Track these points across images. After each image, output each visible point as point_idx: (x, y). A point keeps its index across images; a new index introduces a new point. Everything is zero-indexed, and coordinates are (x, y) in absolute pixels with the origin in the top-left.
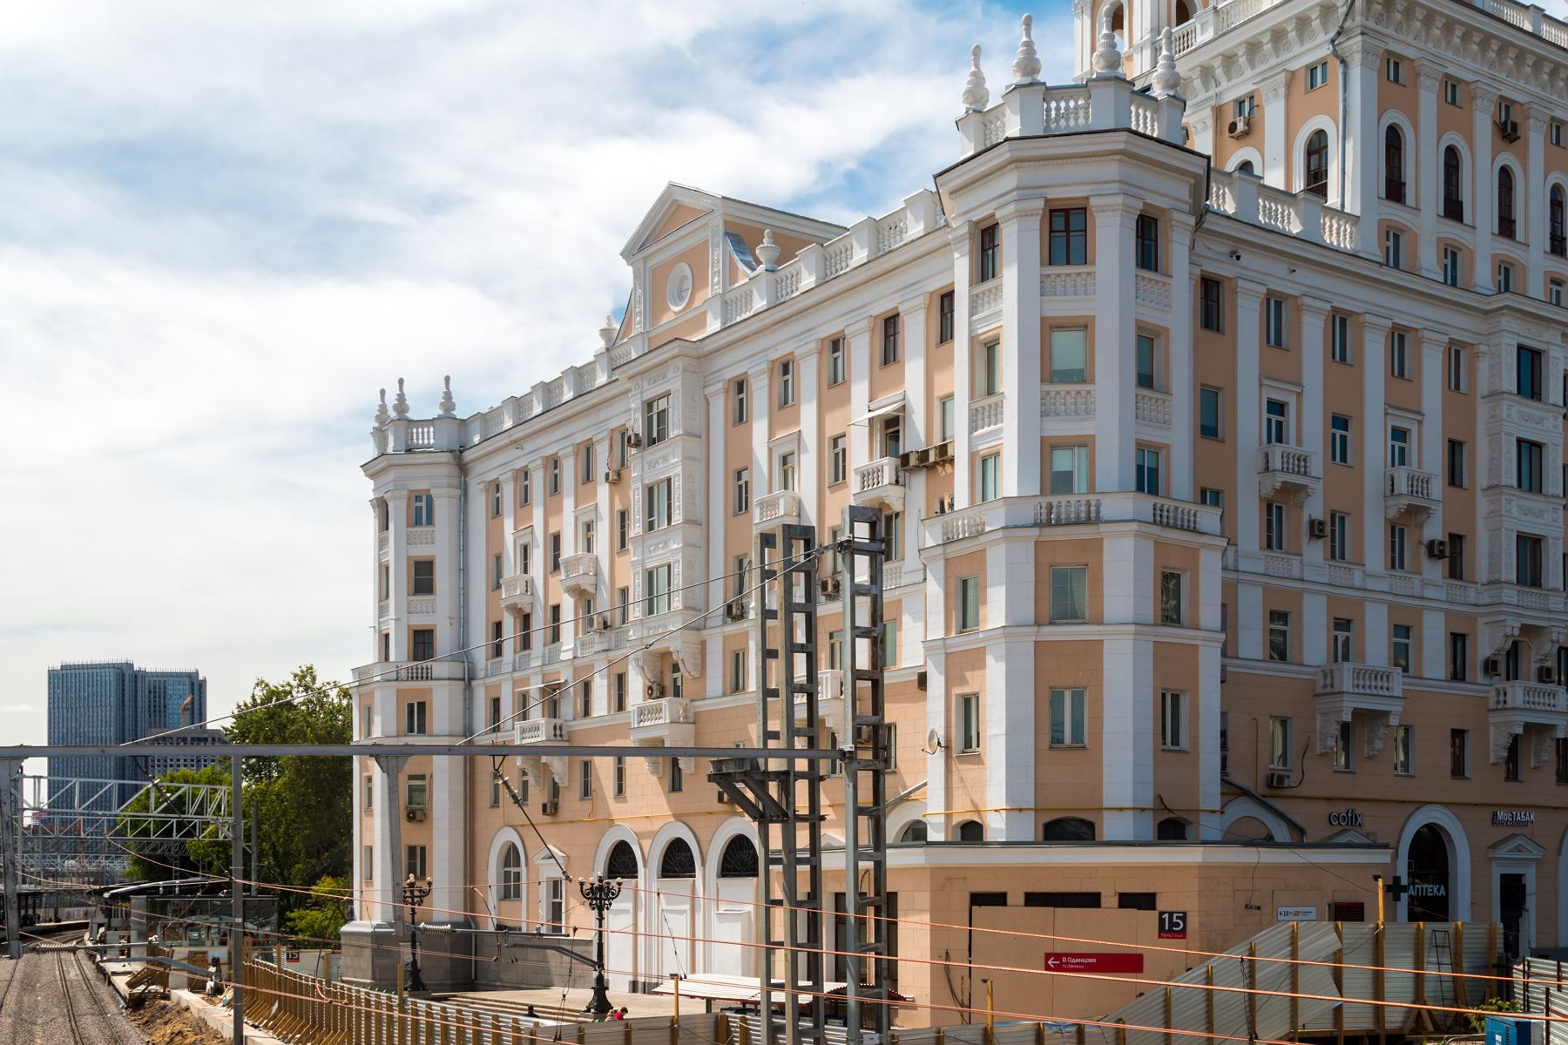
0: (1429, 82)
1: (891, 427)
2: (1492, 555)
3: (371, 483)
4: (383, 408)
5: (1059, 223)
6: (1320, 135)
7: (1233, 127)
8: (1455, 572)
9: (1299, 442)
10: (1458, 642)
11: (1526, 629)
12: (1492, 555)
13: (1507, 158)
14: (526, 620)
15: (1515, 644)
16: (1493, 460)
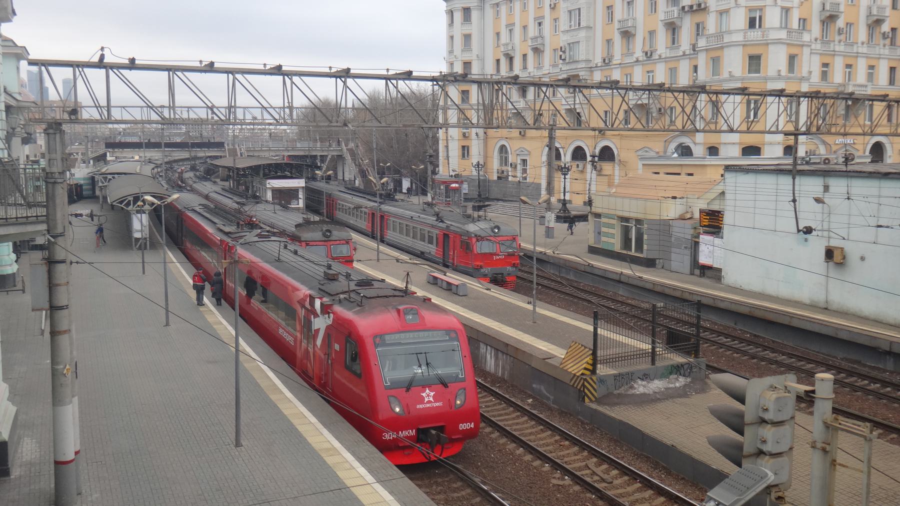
8: (893, 43)
14: (511, 59)
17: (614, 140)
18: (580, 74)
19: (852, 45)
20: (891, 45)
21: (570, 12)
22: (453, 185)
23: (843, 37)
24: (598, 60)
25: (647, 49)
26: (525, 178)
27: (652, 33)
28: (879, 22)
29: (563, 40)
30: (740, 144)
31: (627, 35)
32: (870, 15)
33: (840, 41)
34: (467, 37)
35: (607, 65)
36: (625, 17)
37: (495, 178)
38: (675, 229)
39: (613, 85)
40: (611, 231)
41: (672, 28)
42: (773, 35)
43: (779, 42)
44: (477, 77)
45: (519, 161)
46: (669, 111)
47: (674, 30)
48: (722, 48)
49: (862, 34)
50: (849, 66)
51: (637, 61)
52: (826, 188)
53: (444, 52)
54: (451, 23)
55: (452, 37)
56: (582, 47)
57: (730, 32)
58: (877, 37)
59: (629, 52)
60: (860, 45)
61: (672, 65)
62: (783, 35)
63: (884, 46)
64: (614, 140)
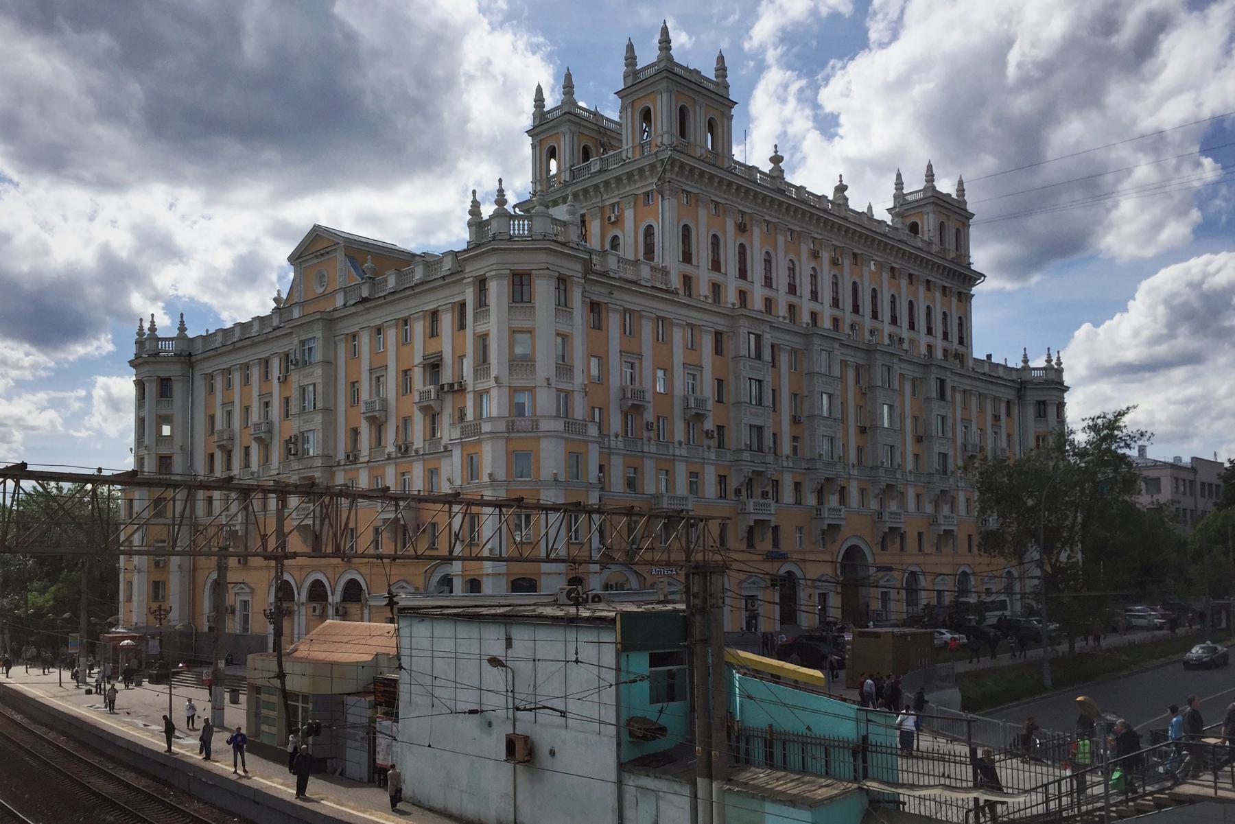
0: (355, 744)
1: (433, 366)
2: (739, 436)
4: (141, 328)
5: (517, 280)
6: (650, 227)
7: (609, 218)
8: (721, 445)
9: (641, 384)
10: (722, 479)
12: (739, 436)
13: (742, 240)
14: (229, 454)
15: (750, 480)
17: (363, 570)
20: (719, 447)
23: (653, 434)
24: (341, 456)
27: (407, 421)
28: (700, 417)
30: (507, 574)
31: (378, 424)
32: (687, 407)
33: (649, 440)
37: (206, 629)
39: (383, 494)
40: (273, 714)
41: (432, 416)
42: (546, 425)
44: (178, 478)
45: (238, 605)
46: (429, 530)
47: (434, 416)
51: (389, 458)
52: (509, 643)
60: (677, 445)
63: (709, 448)
64: (363, 570)
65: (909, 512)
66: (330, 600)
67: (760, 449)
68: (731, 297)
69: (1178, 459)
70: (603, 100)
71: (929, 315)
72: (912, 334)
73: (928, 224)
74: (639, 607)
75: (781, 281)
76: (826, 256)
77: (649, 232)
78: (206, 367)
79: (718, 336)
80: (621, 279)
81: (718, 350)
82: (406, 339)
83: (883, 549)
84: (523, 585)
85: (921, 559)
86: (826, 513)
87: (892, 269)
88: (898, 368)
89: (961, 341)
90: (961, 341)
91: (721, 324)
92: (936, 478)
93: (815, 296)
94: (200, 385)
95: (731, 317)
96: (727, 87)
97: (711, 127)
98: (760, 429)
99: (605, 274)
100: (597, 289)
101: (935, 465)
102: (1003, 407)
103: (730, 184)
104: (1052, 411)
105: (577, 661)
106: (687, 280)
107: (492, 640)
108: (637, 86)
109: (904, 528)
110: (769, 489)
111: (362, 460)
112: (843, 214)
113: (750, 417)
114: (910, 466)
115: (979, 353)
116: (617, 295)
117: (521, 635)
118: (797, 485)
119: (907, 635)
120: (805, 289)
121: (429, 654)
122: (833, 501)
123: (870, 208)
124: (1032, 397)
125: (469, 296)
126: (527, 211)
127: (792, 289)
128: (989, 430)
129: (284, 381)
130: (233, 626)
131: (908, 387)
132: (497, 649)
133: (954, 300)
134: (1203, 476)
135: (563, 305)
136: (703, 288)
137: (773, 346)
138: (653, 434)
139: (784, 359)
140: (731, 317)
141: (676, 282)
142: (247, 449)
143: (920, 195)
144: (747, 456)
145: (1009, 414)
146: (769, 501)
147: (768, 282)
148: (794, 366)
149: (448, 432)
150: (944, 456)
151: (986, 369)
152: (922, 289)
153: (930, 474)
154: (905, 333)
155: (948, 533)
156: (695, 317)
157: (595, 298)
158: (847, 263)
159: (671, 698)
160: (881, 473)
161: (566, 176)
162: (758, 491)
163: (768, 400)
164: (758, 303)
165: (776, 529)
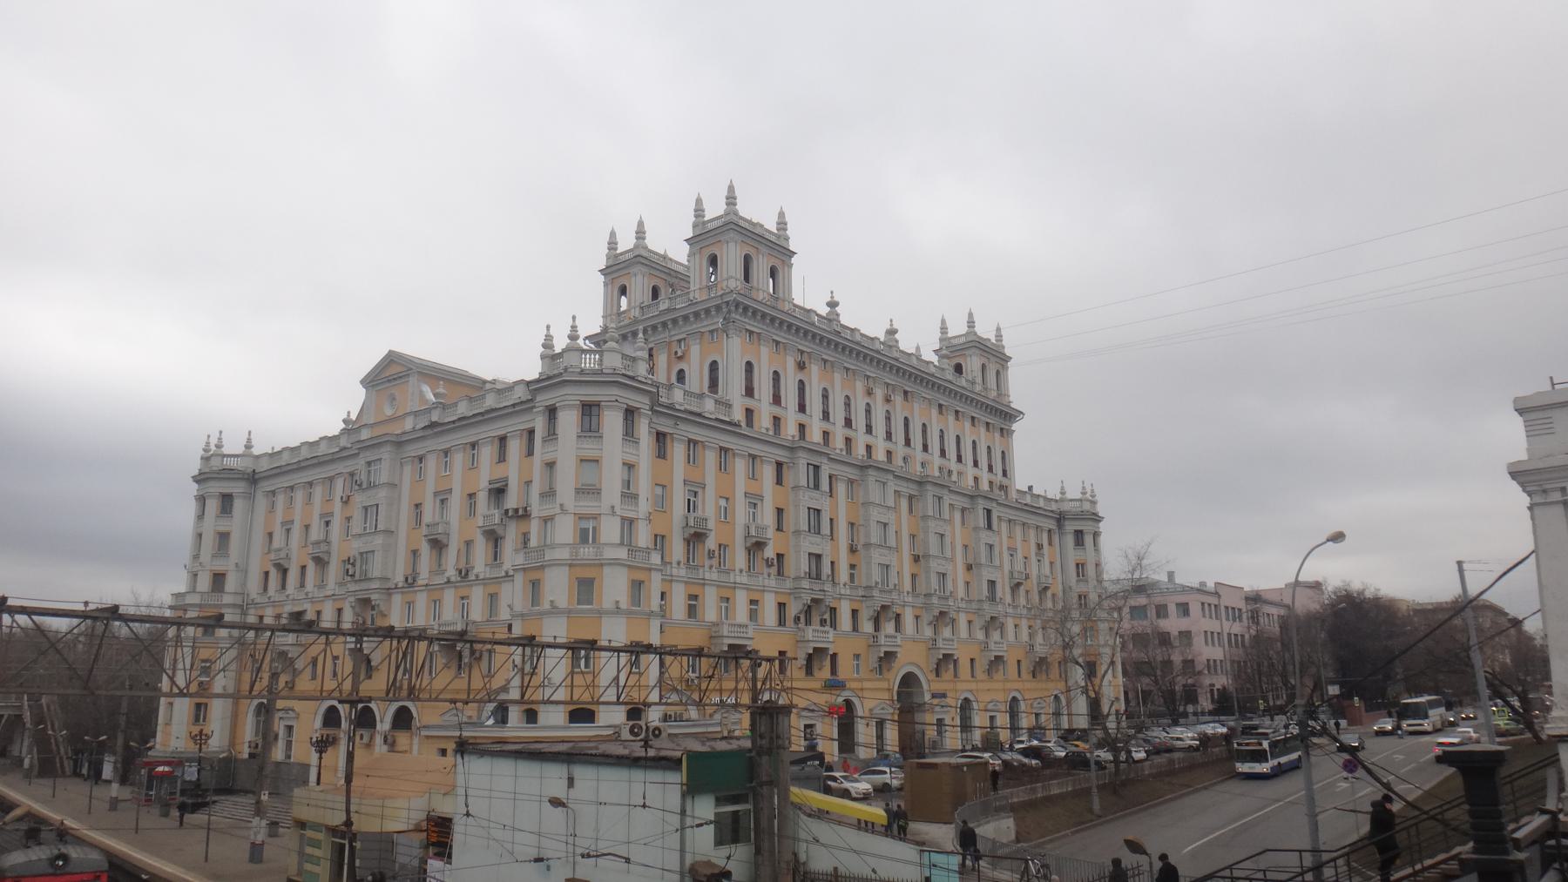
2: (798, 564)
3: (195, 486)
4: (208, 444)
8: (780, 573)
11: (813, 600)
12: (798, 564)
14: (284, 572)
16: (798, 518)
18: (373, 597)
19: (727, 572)
21: (366, 508)
22: (160, 769)
23: (715, 562)
24: (399, 579)
25: (462, 565)
26: (289, 757)
27: (469, 544)
28: (760, 545)
29: (356, 546)
31: (438, 545)
32: (748, 536)
34: (224, 537)
35: (411, 585)
36: (437, 519)
37: (246, 756)
38: (400, 849)
40: (317, 852)
41: (494, 538)
42: (609, 553)
43: (616, 563)
47: (496, 541)
48: (542, 567)
49: (740, 559)
50: (753, 602)
51: (449, 582)
52: (571, 782)
53: (186, 556)
54: (201, 516)
55: (200, 535)
56: (378, 557)
57: (553, 547)
58: (760, 565)
59: (438, 569)
61: (491, 589)
62: (622, 554)
65: (962, 640)
66: (379, 726)
67: (818, 577)
68: (790, 430)
69: (1203, 584)
70: (671, 242)
71: (974, 448)
72: (960, 466)
73: (973, 364)
74: (703, 743)
75: (838, 415)
76: (879, 393)
77: (714, 366)
78: (266, 486)
79: (779, 465)
80: (686, 411)
81: (779, 481)
82: (473, 465)
83: (937, 675)
84: (581, 715)
85: (973, 686)
86: (882, 640)
87: (940, 406)
88: (948, 499)
89: (1005, 474)
90: (1005, 474)
91: (781, 455)
92: (986, 606)
93: (869, 429)
94: (261, 503)
95: (792, 449)
96: (787, 239)
97: (773, 273)
98: (819, 557)
99: (671, 407)
100: (662, 420)
101: (985, 592)
102: (1045, 536)
103: (837, 344)
104: (1088, 540)
105: (644, 806)
106: (749, 412)
107: (553, 778)
108: (706, 237)
109: (957, 654)
110: (827, 616)
111: (420, 582)
112: (895, 355)
113: (810, 544)
114: (961, 593)
115: (1020, 481)
116: (682, 426)
117: (583, 773)
118: (854, 612)
119: (963, 765)
120: (860, 421)
121: (486, 793)
122: (889, 628)
123: (918, 348)
124: (1070, 527)
125: (540, 424)
126: (597, 344)
127: (848, 423)
128: (1033, 558)
129: (346, 501)
130: (278, 754)
131: (957, 515)
132: (559, 790)
133: (997, 435)
134: (1226, 601)
135: (629, 433)
136: (764, 422)
137: (830, 477)
138: (715, 562)
139: (841, 489)
140: (792, 449)
141: (738, 415)
142: (304, 568)
143: (963, 340)
144: (805, 584)
145: (1050, 544)
146: (827, 628)
147: (826, 416)
148: (851, 495)
149: (511, 557)
150: (992, 583)
151: (1028, 500)
152: (983, 430)
153: (980, 601)
154: (953, 464)
155: (998, 658)
156: (756, 449)
157: (661, 429)
158: (898, 399)
159: (735, 840)
160: (935, 600)
161: (636, 313)
162: (816, 619)
163: (826, 529)
164: (815, 436)
165: (834, 656)
